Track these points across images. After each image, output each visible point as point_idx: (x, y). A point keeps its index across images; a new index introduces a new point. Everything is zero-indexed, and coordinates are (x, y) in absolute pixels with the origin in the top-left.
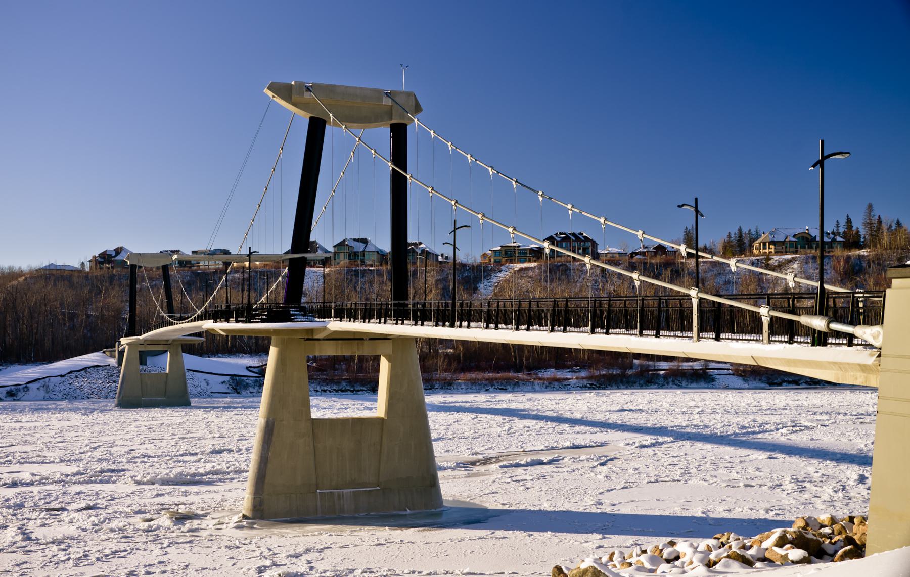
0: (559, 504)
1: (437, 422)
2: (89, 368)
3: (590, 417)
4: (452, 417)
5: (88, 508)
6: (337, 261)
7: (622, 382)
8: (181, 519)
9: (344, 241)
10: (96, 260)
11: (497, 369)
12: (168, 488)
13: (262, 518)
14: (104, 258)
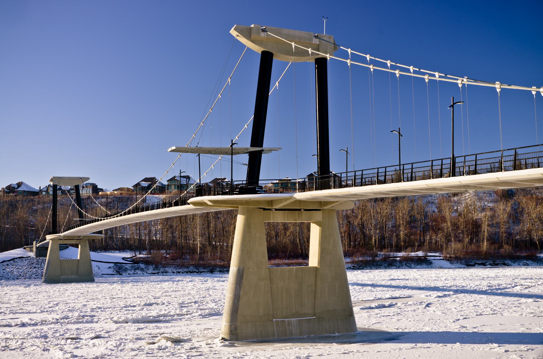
2: (16, 258)
6: (170, 190)
7: (373, 265)
9: (175, 177)
10: (4, 191)
13: (237, 340)
14: (9, 189)
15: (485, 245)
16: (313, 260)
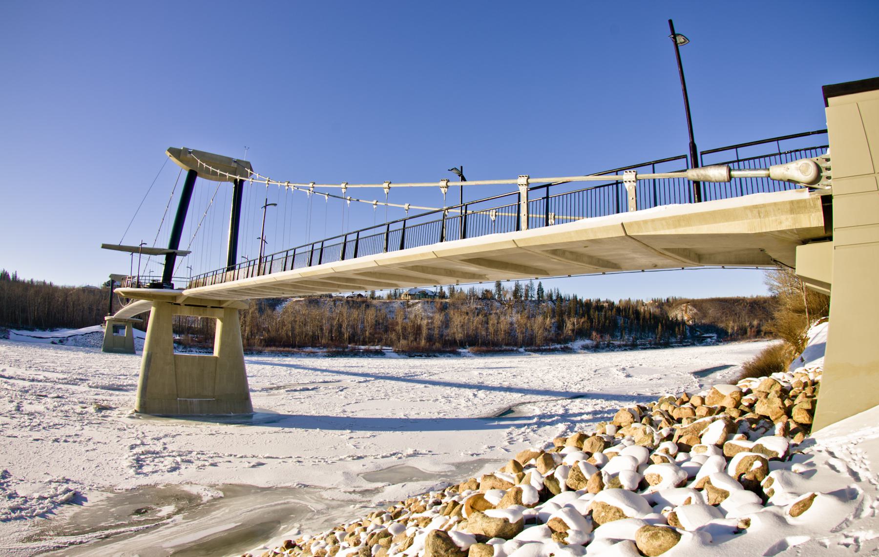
0: (321, 412)
1: (250, 369)
3: (330, 369)
4: (261, 367)
5: (58, 397)
8: (101, 409)
11: (285, 346)
12: (104, 391)
15: (423, 342)
16: (216, 353)
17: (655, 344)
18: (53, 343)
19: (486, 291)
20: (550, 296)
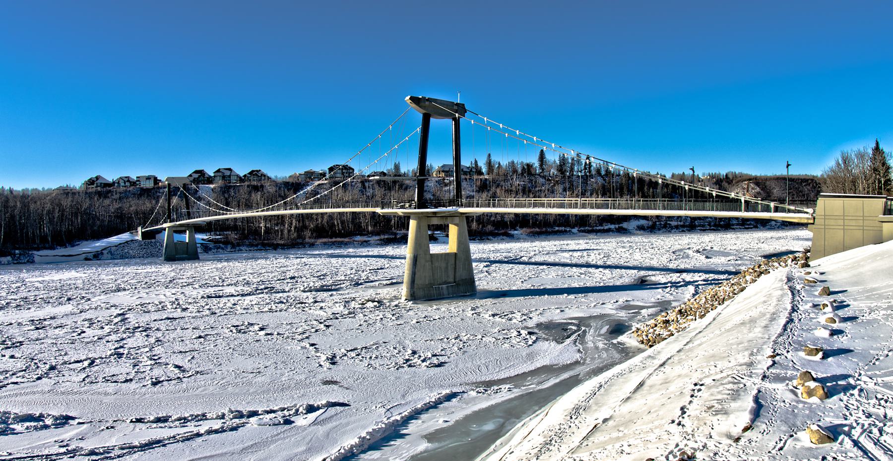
17: (715, 226)
18: (86, 259)
19: (528, 165)
20: (598, 171)
